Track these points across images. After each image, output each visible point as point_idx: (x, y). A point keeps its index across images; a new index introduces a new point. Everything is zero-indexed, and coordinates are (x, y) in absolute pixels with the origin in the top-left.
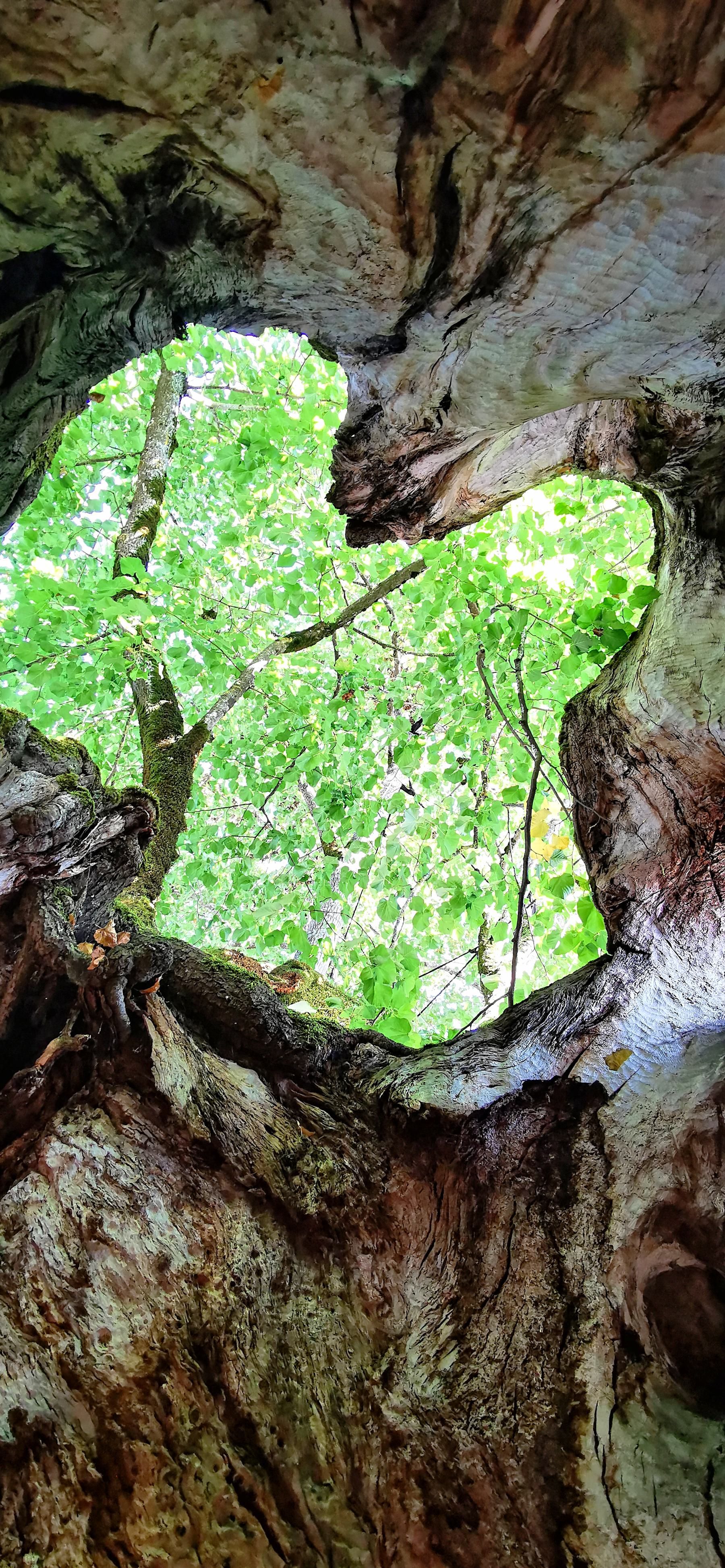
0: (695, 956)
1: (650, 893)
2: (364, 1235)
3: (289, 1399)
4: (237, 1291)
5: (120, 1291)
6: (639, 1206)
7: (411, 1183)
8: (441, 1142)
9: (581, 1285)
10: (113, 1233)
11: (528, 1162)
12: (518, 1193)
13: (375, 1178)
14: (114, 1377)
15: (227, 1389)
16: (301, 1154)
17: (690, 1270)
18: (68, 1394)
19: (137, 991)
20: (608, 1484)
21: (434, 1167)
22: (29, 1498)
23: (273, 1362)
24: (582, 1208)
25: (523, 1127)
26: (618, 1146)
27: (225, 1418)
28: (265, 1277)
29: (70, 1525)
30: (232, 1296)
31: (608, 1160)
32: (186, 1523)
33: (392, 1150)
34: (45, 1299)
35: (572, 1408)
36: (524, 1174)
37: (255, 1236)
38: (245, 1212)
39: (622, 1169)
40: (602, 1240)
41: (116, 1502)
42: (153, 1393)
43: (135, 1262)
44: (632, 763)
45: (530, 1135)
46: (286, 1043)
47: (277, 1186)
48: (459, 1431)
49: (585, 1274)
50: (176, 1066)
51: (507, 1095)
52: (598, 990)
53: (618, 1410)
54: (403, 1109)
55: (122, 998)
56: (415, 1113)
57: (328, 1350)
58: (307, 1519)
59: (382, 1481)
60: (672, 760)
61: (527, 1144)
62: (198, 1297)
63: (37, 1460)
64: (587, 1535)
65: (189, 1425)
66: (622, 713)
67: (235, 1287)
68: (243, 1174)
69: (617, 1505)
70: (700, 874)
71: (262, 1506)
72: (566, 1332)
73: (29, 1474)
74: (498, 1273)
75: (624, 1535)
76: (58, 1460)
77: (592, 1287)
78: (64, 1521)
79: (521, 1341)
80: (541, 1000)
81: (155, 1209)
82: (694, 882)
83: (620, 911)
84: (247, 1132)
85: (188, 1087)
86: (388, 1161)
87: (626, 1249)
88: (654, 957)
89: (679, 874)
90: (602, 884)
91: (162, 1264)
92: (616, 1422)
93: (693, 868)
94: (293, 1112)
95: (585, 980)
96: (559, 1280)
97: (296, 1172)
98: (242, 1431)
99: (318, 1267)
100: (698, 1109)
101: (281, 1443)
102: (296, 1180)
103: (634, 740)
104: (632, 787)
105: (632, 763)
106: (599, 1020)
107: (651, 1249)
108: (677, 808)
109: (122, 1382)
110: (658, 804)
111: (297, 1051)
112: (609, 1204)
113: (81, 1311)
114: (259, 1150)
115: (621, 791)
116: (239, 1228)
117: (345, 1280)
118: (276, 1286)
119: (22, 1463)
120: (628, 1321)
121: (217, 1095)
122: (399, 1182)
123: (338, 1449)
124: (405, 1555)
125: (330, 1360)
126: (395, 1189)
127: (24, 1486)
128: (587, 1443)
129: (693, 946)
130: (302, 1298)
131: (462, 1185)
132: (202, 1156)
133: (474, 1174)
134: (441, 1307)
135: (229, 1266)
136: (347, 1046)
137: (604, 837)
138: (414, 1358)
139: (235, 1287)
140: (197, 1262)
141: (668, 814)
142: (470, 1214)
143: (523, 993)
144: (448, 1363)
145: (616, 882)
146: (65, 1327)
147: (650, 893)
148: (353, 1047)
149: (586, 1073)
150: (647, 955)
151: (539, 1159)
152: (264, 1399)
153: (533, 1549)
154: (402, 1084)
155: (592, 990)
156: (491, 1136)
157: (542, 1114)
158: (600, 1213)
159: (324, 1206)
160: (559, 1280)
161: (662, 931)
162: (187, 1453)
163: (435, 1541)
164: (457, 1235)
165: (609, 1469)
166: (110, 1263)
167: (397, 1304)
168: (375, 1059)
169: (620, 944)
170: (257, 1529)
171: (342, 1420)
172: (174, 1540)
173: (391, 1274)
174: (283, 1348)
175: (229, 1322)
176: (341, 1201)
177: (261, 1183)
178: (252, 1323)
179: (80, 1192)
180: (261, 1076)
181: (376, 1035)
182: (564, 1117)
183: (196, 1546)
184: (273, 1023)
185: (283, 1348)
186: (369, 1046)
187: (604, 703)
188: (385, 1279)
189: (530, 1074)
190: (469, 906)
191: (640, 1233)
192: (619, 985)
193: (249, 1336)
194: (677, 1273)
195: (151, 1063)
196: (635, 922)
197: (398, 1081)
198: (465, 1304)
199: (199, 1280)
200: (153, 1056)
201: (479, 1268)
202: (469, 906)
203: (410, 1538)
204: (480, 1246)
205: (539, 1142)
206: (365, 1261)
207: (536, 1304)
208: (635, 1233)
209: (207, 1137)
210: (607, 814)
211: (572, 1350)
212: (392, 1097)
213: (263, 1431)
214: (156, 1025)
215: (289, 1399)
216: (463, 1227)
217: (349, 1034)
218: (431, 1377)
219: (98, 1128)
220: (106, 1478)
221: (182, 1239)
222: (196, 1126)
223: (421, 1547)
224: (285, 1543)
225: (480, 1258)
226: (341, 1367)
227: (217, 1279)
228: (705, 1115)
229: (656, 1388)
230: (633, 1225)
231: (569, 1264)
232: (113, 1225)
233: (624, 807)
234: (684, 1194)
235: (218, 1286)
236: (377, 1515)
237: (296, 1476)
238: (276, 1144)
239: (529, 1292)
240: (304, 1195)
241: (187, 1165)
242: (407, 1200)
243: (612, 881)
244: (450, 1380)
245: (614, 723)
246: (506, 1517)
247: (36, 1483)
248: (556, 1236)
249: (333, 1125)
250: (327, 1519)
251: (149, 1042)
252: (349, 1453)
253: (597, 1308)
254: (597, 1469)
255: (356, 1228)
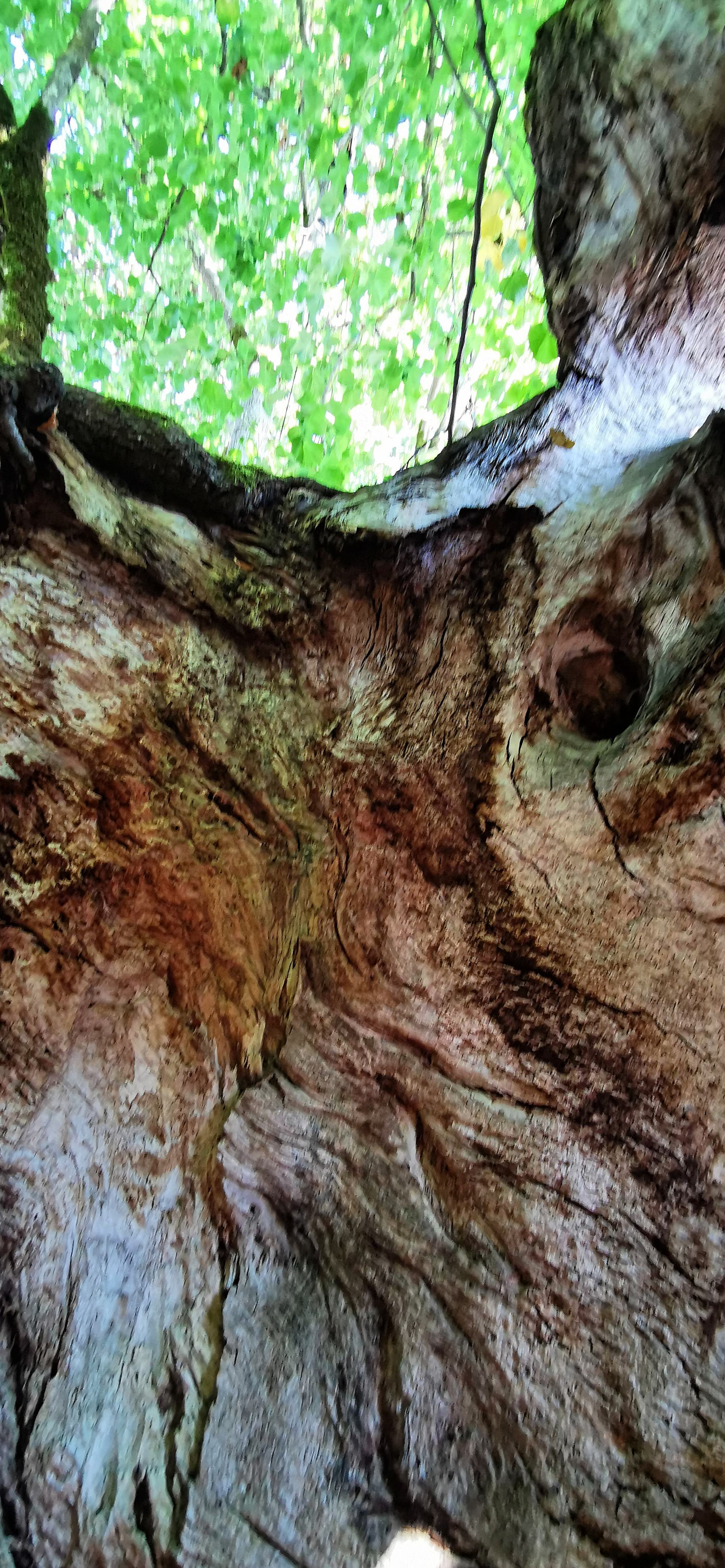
0: (650, 380)
1: (613, 305)
2: (309, 646)
3: (253, 751)
4: (196, 684)
5: (86, 683)
6: (562, 601)
7: (351, 602)
8: (379, 564)
9: (504, 663)
10: (67, 643)
11: (463, 578)
12: (451, 603)
13: (317, 599)
14: (95, 739)
15: (198, 746)
16: (241, 580)
17: (599, 654)
18: (57, 751)
19: (32, 423)
20: (515, 777)
21: (373, 588)
22: (42, 812)
23: (235, 730)
24: (511, 610)
25: (456, 550)
26: (548, 556)
27: (200, 763)
28: (219, 675)
29: (81, 826)
30: (191, 688)
31: (537, 569)
32: (179, 823)
33: (330, 575)
34: (15, 689)
35: (489, 740)
36: (458, 587)
37: (205, 647)
38: (195, 631)
39: (550, 575)
40: (526, 631)
41: (117, 812)
42: (133, 748)
43: (94, 664)
44: (616, 110)
45: (464, 555)
46: (213, 486)
47: (221, 609)
48: (397, 759)
49: (507, 656)
50: (95, 503)
51: (443, 520)
52: (542, 419)
53: (528, 737)
54: (340, 534)
55: (19, 438)
56: (351, 536)
57: (284, 723)
58: (277, 818)
59: (335, 793)
60: (669, 100)
61: (462, 563)
62: (161, 688)
63: (41, 787)
64: (496, 808)
65: (168, 766)
66: (612, 32)
67: (193, 679)
68: (185, 598)
69: (521, 788)
70: (675, 273)
71: (239, 812)
72: (489, 691)
73: (37, 798)
74: (431, 663)
75: (524, 803)
76: (60, 788)
77: (514, 665)
78: (76, 824)
79: (450, 703)
80: (482, 436)
81: (104, 626)
82: (665, 286)
83: (576, 328)
84: (183, 564)
85: (113, 520)
86: (328, 585)
87: (547, 634)
88: (606, 384)
89: (651, 274)
90: (559, 296)
91: (121, 664)
92: (525, 744)
93: (668, 265)
94: (229, 551)
95: (530, 411)
96: (486, 662)
97: (238, 596)
98: (216, 771)
99: (268, 667)
100: (630, 517)
101: (250, 776)
102: (239, 602)
103: (623, 73)
104: (611, 151)
105: (616, 110)
106: (541, 449)
107: (567, 637)
108: (663, 176)
109: (103, 742)
110: (642, 172)
111: (226, 493)
112: (535, 604)
113: (52, 697)
114: (197, 580)
115: (597, 161)
116: (191, 644)
117: (295, 675)
118: (231, 681)
119: (30, 789)
120: (541, 684)
121: (146, 531)
122: (339, 602)
123: (298, 779)
124: (356, 831)
125: (285, 728)
126: (336, 607)
127: (35, 803)
128: (501, 757)
129: (650, 371)
130: (255, 690)
131: (399, 599)
132: (143, 584)
133: (411, 588)
134: (380, 690)
135: (185, 667)
136: (277, 492)
137: (568, 234)
138: (358, 721)
139: (193, 679)
140: (155, 665)
141: (650, 186)
142: (407, 623)
143: (464, 425)
144: (387, 722)
145: (577, 290)
146: (40, 708)
147: (613, 305)
148: (285, 492)
149: (523, 499)
150: (598, 381)
151: (472, 575)
152: (232, 751)
153: (454, 819)
154: (338, 514)
155: (536, 421)
156: (427, 559)
157: (478, 537)
158: (526, 612)
159: (268, 621)
160: (486, 662)
161: (619, 352)
162: (172, 783)
163: (379, 820)
164: (395, 639)
165: (516, 770)
166: (69, 663)
167: (341, 692)
168: (309, 502)
169: (571, 368)
170: (239, 826)
171: (300, 764)
172: (171, 833)
173: (336, 673)
174: (243, 721)
175: (191, 704)
176: (285, 616)
177: (204, 605)
178: (213, 705)
179: (23, 611)
180: (192, 520)
181: (308, 480)
182: (499, 539)
183: (190, 836)
184: (195, 465)
185: (243, 721)
186: (301, 491)
187: (588, 20)
188: (330, 675)
189: (469, 501)
190: (404, 377)
191: (561, 622)
192: (565, 414)
193: (211, 713)
194: (589, 657)
195: (67, 498)
196: (591, 341)
197: (333, 513)
198: (401, 687)
199: (159, 678)
200: (67, 489)
201: (414, 661)
202: (404, 377)
203: (360, 819)
204: (416, 645)
205: (474, 562)
206: (311, 665)
207: (464, 679)
208: (555, 622)
209: (143, 563)
210: (576, 195)
211: (493, 705)
212: (328, 524)
213: (233, 770)
214: (65, 462)
215: (253, 751)
216: (400, 631)
217: (277, 480)
218: (373, 731)
219: (26, 561)
220: (104, 797)
221: (136, 648)
222: (128, 553)
223: (368, 824)
224: (261, 832)
225: (416, 653)
226: (296, 733)
227: (176, 676)
228: (635, 521)
229: (560, 726)
230: (555, 615)
231: (495, 650)
232: (64, 636)
233: (597, 186)
234: (603, 589)
235: (177, 681)
236: (333, 814)
237: (264, 795)
238: (214, 575)
239: (458, 672)
240: (248, 613)
241: (128, 593)
242: (347, 617)
243: (572, 288)
244: (389, 732)
245: (600, 50)
246: (435, 803)
247: (45, 801)
248: (484, 632)
249: (270, 560)
250: (294, 818)
251: (60, 478)
252: (307, 781)
253: (516, 677)
254: (507, 770)
255: (301, 640)
